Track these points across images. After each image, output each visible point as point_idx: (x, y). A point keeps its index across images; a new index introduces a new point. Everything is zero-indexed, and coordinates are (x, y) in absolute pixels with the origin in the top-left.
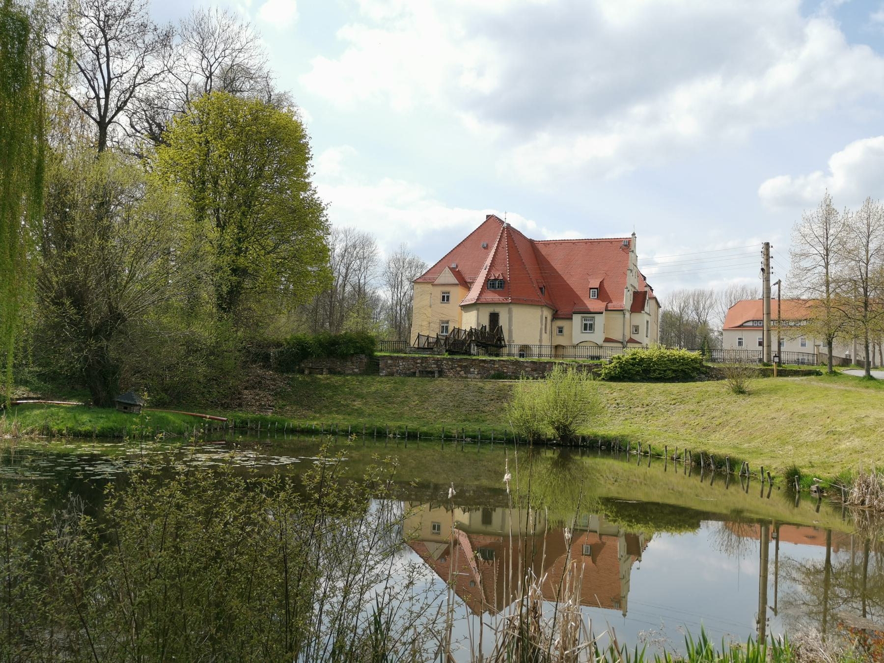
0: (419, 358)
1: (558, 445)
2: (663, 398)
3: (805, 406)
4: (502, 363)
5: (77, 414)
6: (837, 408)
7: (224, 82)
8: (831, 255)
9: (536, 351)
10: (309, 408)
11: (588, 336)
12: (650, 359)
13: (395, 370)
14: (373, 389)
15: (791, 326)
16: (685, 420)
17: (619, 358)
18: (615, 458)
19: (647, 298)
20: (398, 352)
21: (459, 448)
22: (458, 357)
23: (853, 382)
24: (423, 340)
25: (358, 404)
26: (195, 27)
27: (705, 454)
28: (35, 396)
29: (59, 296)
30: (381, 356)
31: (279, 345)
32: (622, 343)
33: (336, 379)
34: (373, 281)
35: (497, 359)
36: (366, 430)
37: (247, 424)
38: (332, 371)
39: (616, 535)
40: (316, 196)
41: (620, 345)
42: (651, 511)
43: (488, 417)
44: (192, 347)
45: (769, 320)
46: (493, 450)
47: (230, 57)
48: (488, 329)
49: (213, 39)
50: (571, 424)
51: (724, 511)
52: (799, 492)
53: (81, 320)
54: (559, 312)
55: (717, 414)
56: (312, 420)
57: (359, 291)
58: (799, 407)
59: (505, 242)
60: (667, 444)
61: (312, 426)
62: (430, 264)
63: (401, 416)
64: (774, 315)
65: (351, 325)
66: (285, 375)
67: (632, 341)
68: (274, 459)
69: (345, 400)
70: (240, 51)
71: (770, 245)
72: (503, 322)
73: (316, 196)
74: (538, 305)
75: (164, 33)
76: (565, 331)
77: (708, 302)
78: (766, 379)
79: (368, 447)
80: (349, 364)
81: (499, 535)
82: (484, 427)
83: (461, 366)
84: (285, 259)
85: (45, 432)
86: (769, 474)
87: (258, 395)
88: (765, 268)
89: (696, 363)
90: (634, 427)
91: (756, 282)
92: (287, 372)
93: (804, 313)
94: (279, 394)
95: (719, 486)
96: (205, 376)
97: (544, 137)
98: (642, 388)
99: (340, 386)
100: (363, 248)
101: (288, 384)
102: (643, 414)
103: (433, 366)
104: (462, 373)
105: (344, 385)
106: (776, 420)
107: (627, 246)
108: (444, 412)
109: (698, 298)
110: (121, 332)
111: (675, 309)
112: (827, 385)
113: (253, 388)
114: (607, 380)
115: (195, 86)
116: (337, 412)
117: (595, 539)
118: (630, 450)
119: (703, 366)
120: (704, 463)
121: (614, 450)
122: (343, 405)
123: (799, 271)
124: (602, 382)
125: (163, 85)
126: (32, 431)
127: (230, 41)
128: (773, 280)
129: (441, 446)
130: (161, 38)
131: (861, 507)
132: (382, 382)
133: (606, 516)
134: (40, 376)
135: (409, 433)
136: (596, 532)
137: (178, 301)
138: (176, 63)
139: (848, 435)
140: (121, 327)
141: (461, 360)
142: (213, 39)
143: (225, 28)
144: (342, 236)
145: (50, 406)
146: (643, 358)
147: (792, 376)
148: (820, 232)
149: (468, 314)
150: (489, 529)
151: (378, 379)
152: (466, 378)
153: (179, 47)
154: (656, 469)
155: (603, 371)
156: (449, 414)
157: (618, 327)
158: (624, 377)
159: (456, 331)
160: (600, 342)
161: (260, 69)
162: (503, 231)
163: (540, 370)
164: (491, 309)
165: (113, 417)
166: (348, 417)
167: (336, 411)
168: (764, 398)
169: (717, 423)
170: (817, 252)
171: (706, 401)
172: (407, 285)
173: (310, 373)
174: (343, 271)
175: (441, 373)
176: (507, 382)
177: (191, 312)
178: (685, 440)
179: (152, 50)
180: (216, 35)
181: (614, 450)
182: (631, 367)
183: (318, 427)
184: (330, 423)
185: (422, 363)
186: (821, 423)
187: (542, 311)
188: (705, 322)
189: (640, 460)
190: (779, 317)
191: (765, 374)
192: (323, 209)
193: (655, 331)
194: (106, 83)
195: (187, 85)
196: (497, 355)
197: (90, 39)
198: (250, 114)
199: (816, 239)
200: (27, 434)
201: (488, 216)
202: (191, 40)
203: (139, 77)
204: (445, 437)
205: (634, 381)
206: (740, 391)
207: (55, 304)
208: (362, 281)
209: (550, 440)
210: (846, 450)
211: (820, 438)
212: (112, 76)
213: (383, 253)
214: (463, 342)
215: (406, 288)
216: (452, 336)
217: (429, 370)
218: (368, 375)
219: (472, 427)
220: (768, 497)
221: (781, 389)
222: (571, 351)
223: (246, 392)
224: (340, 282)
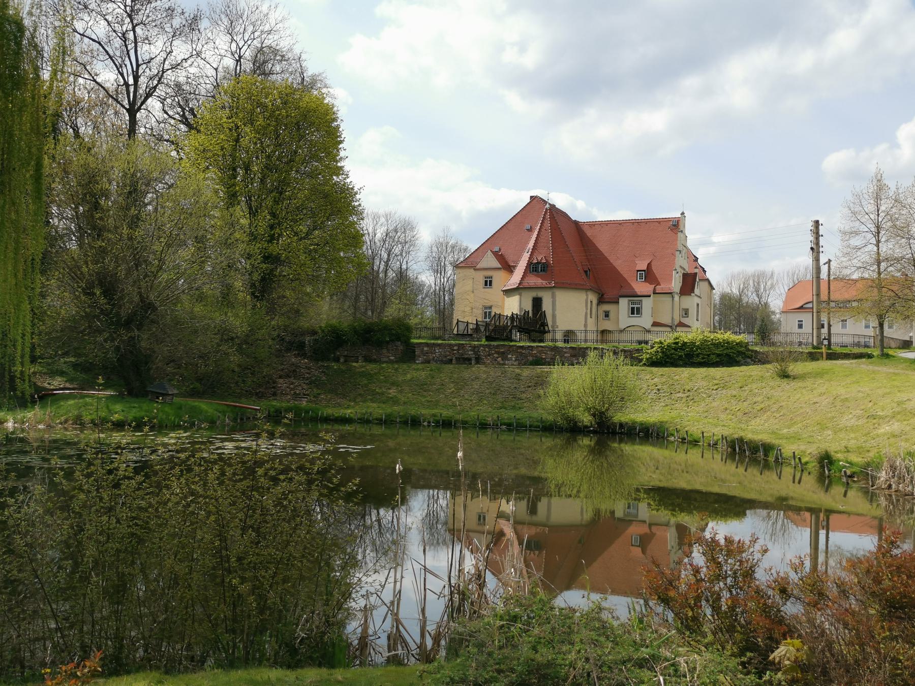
0: (456, 345)
1: (595, 432)
2: (705, 383)
3: (849, 390)
4: (540, 349)
5: (110, 404)
6: (880, 392)
7: (254, 65)
8: (882, 232)
9: (580, 336)
10: (344, 396)
11: (635, 321)
12: (693, 343)
13: (431, 357)
14: (409, 376)
15: (840, 308)
16: (726, 405)
17: (661, 343)
18: (653, 445)
19: (697, 280)
20: (437, 339)
21: (495, 436)
22: (495, 343)
23: (904, 365)
24: (462, 327)
25: (393, 392)
26: (223, 10)
27: (741, 440)
28: (71, 387)
29: (90, 285)
30: (417, 344)
31: (314, 333)
32: (671, 327)
33: (371, 367)
34: (415, 267)
35: (542, 344)
36: (400, 418)
37: (281, 413)
38: (368, 359)
39: (667, 525)
40: (348, 180)
41: (669, 329)
42: (695, 500)
43: (525, 405)
44: (226, 335)
45: (819, 302)
46: (529, 437)
47: (259, 39)
48: (531, 315)
49: (241, 21)
50: (607, 410)
51: (769, 499)
52: (829, 477)
53: (112, 310)
54: (605, 296)
55: (759, 399)
56: (346, 408)
57: (402, 276)
58: (842, 391)
59: (548, 224)
60: (704, 430)
61: (346, 414)
62: (473, 247)
63: (436, 404)
64: (824, 296)
65: (392, 311)
66: (320, 363)
67: (681, 324)
68: (301, 447)
69: (380, 388)
70: (269, 32)
71: (820, 223)
72: (546, 306)
73: (348, 180)
74: (583, 289)
75: (192, 16)
76: (611, 315)
77: (769, 283)
78: (813, 363)
79: (404, 435)
80: (385, 351)
81: (545, 526)
82: (519, 414)
83: (498, 353)
84: (318, 245)
85: (78, 422)
86: (800, 459)
87: (292, 383)
88: (814, 247)
89: (741, 346)
90: (674, 414)
91: (807, 260)
92: (322, 360)
93: (854, 293)
94: (314, 383)
95: (754, 471)
96: (239, 366)
97: (591, 113)
98: (685, 373)
99: (375, 374)
100: (405, 232)
101: (323, 372)
102: (684, 400)
103: (470, 353)
104: (500, 359)
105: (379, 373)
106: (818, 405)
107: (675, 226)
108: (480, 400)
110: (153, 322)
111: (734, 291)
112: (876, 368)
113: (288, 376)
114: (648, 366)
115: (226, 69)
116: (372, 401)
117: (644, 529)
118: (668, 436)
119: (749, 350)
120: (739, 449)
121: (652, 437)
122: (378, 393)
123: (849, 250)
124: (643, 368)
125: (192, 70)
126: (66, 421)
127: (259, 22)
128: (823, 259)
129: (476, 434)
130: (190, 22)
131: (887, 492)
132: (417, 370)
133: (649, 504)
134: (75, 366)
135: (443, 421)
136: (645, 522)
137: (212, 289)
138: (205, 46)
139: (887, 419)
140: (152, 317)
141: (498, 346)
142: (241, 21)
143: (254, 9)
144: (383, 220)
145: (83, 397)
146: (686, 343)
147: (853, 359)
148: (871, 208)
149: (510, 299)
150: (535, 519)
151: (414, 366)
152: (504, 364)
153: (208, 31)
154: (694, 455)
155: (645, 356)
156: (485, 402)
157: (667, 310)
158: (666, 362)
159: (497, 317)
160: (648, 326)
161: (290, 50)
162: (546, 212)
163: (577, 355)
164: (534, 294)
165: (145, 406)
166: (384, 406)
167: (371, 400)
168: (809, 383)
169: (759, 408)
170: (867, 230)
171: (749, 386)
172: (450, 270)
173: (346, 361)
174: (385, 256)
175: (478, 360)
176: (546, 368)
177: (227, 299)
178: (724, 426)
179: (180, 34)
180: (245, 17)
181: (652, 437)
182: (673, 351)
183: (352, 415)
184: (364, 411)
185: (458, 350)
186: (862, 407)
187: (587, 295)
188: (766, 304)
189: (678, 447)
190: (829, 298)
191: (813, 357)
192: (356, 193)
193: (707, 314)
194: (135, 69)
195: (216, 69)
196: (542, 341)
197: (116, 25)
198: (280, 98)
199: (867, 216)
200: (61, 423)
201: (531, 197)
202: (220, 22)
203: (167, 62)
204: (480, 424)
205: (676, 366)
206: (785, 375)
207: (86, 294)
208: (404, 267)
209: (586, 427)
210: (884, 434)
211: (860, 423)
212: (140, 62)
213: (425, 237)
214: (505, 327)
215: (450, 272)
216: (493, 322)
217: (466, 356)
218: (404, 362)
219: (508, 415)
220: (799, 482)
221: (827, 373)
222: (616, 336)
223: (281, 381)
224: (382, 267)
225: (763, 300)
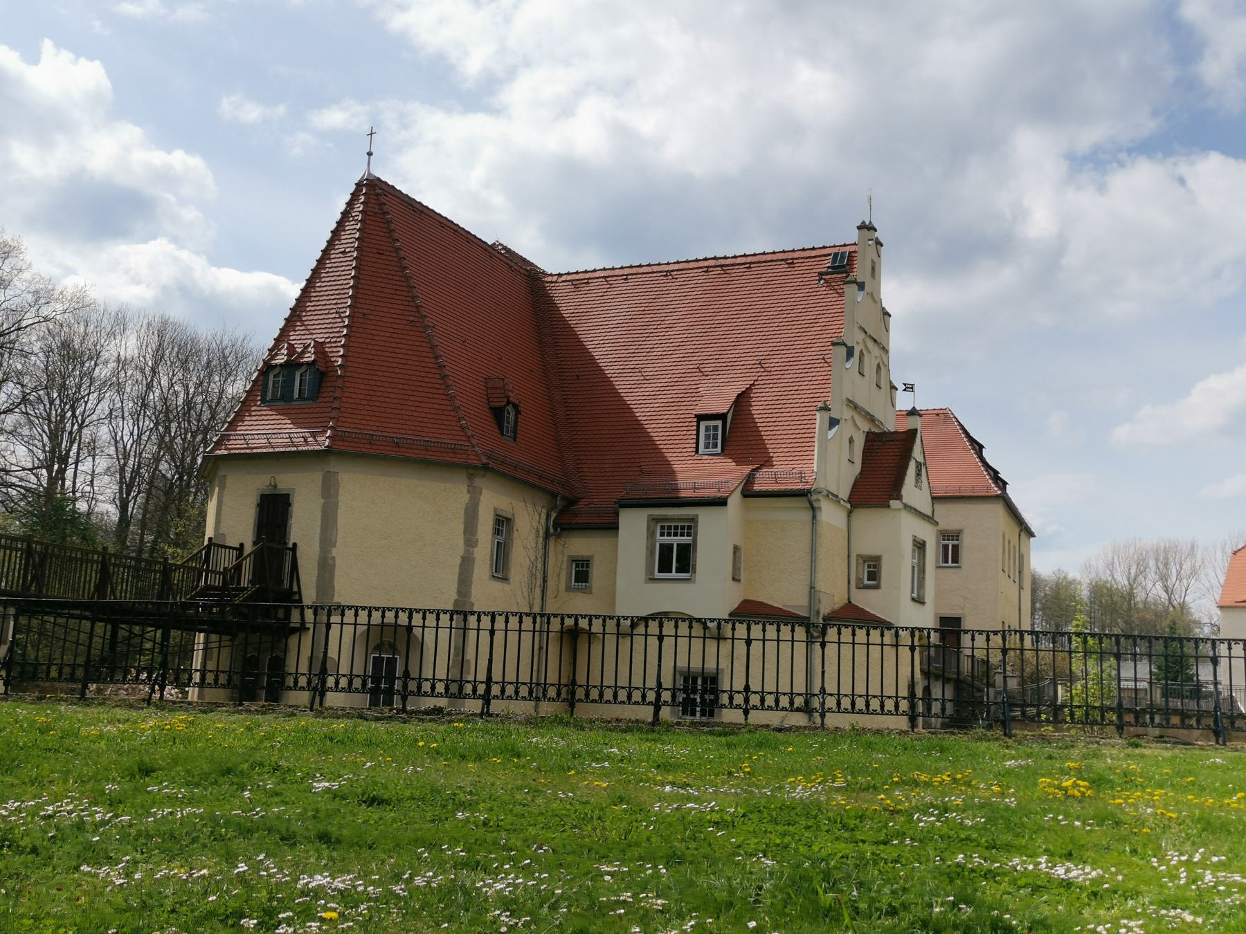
54: (581, 506)
76: (596, 573)
109: (1166, 559)
188: (1183, 606)
225: (1177, 600)
